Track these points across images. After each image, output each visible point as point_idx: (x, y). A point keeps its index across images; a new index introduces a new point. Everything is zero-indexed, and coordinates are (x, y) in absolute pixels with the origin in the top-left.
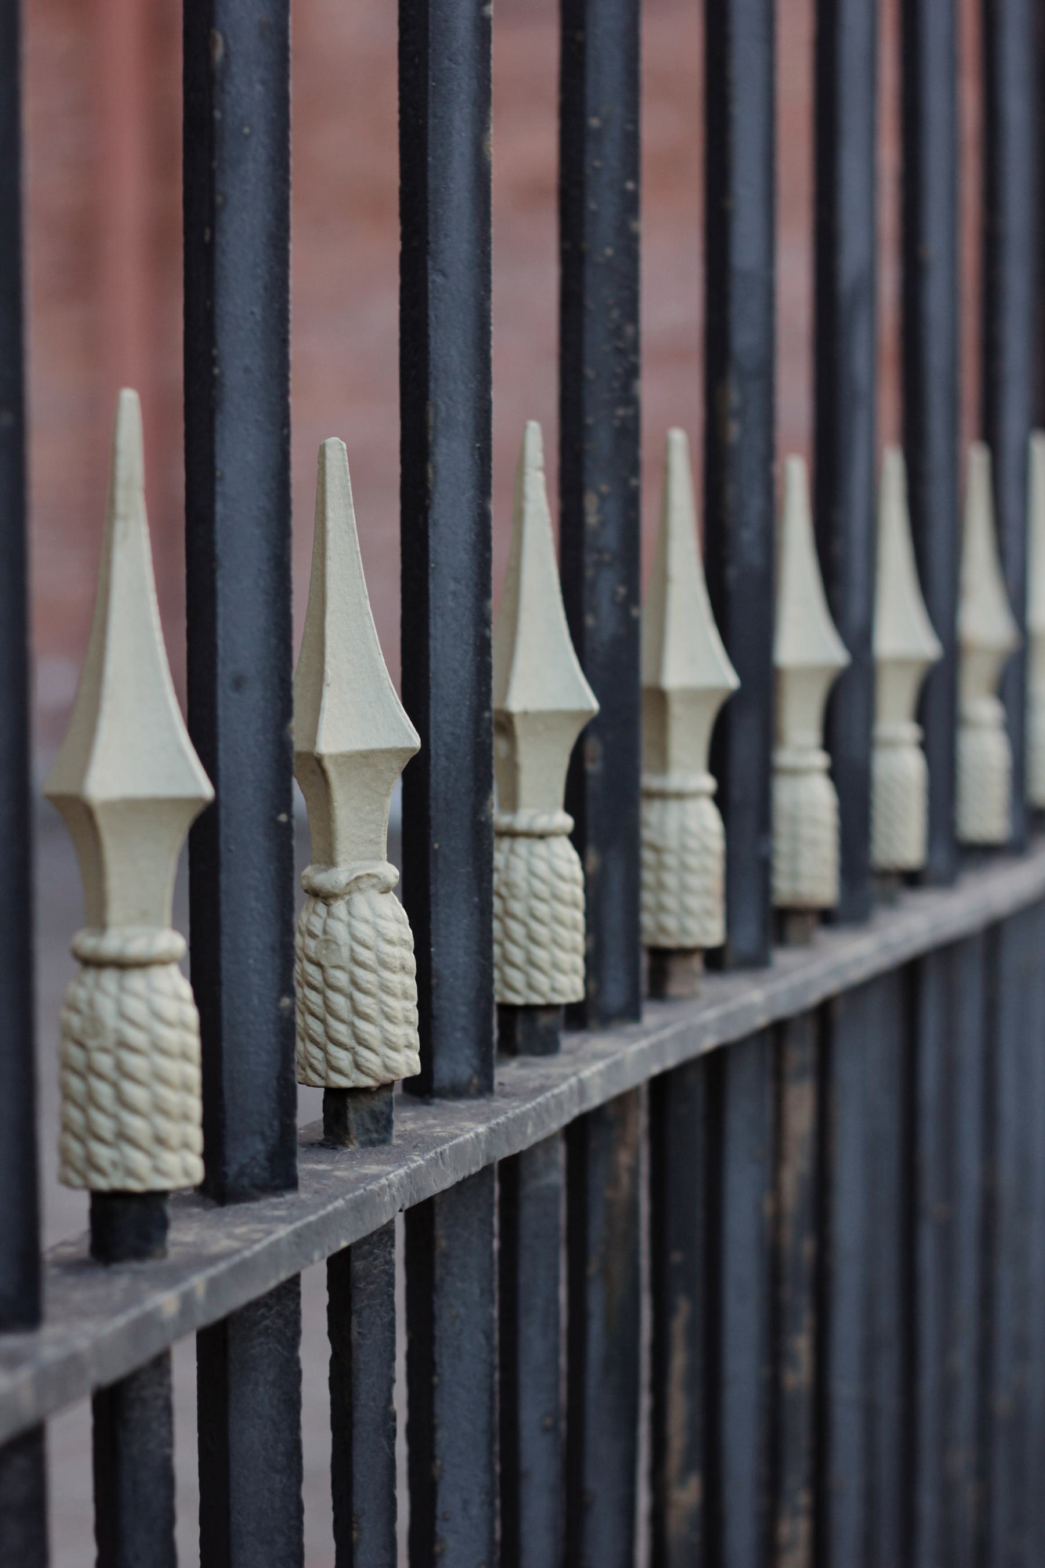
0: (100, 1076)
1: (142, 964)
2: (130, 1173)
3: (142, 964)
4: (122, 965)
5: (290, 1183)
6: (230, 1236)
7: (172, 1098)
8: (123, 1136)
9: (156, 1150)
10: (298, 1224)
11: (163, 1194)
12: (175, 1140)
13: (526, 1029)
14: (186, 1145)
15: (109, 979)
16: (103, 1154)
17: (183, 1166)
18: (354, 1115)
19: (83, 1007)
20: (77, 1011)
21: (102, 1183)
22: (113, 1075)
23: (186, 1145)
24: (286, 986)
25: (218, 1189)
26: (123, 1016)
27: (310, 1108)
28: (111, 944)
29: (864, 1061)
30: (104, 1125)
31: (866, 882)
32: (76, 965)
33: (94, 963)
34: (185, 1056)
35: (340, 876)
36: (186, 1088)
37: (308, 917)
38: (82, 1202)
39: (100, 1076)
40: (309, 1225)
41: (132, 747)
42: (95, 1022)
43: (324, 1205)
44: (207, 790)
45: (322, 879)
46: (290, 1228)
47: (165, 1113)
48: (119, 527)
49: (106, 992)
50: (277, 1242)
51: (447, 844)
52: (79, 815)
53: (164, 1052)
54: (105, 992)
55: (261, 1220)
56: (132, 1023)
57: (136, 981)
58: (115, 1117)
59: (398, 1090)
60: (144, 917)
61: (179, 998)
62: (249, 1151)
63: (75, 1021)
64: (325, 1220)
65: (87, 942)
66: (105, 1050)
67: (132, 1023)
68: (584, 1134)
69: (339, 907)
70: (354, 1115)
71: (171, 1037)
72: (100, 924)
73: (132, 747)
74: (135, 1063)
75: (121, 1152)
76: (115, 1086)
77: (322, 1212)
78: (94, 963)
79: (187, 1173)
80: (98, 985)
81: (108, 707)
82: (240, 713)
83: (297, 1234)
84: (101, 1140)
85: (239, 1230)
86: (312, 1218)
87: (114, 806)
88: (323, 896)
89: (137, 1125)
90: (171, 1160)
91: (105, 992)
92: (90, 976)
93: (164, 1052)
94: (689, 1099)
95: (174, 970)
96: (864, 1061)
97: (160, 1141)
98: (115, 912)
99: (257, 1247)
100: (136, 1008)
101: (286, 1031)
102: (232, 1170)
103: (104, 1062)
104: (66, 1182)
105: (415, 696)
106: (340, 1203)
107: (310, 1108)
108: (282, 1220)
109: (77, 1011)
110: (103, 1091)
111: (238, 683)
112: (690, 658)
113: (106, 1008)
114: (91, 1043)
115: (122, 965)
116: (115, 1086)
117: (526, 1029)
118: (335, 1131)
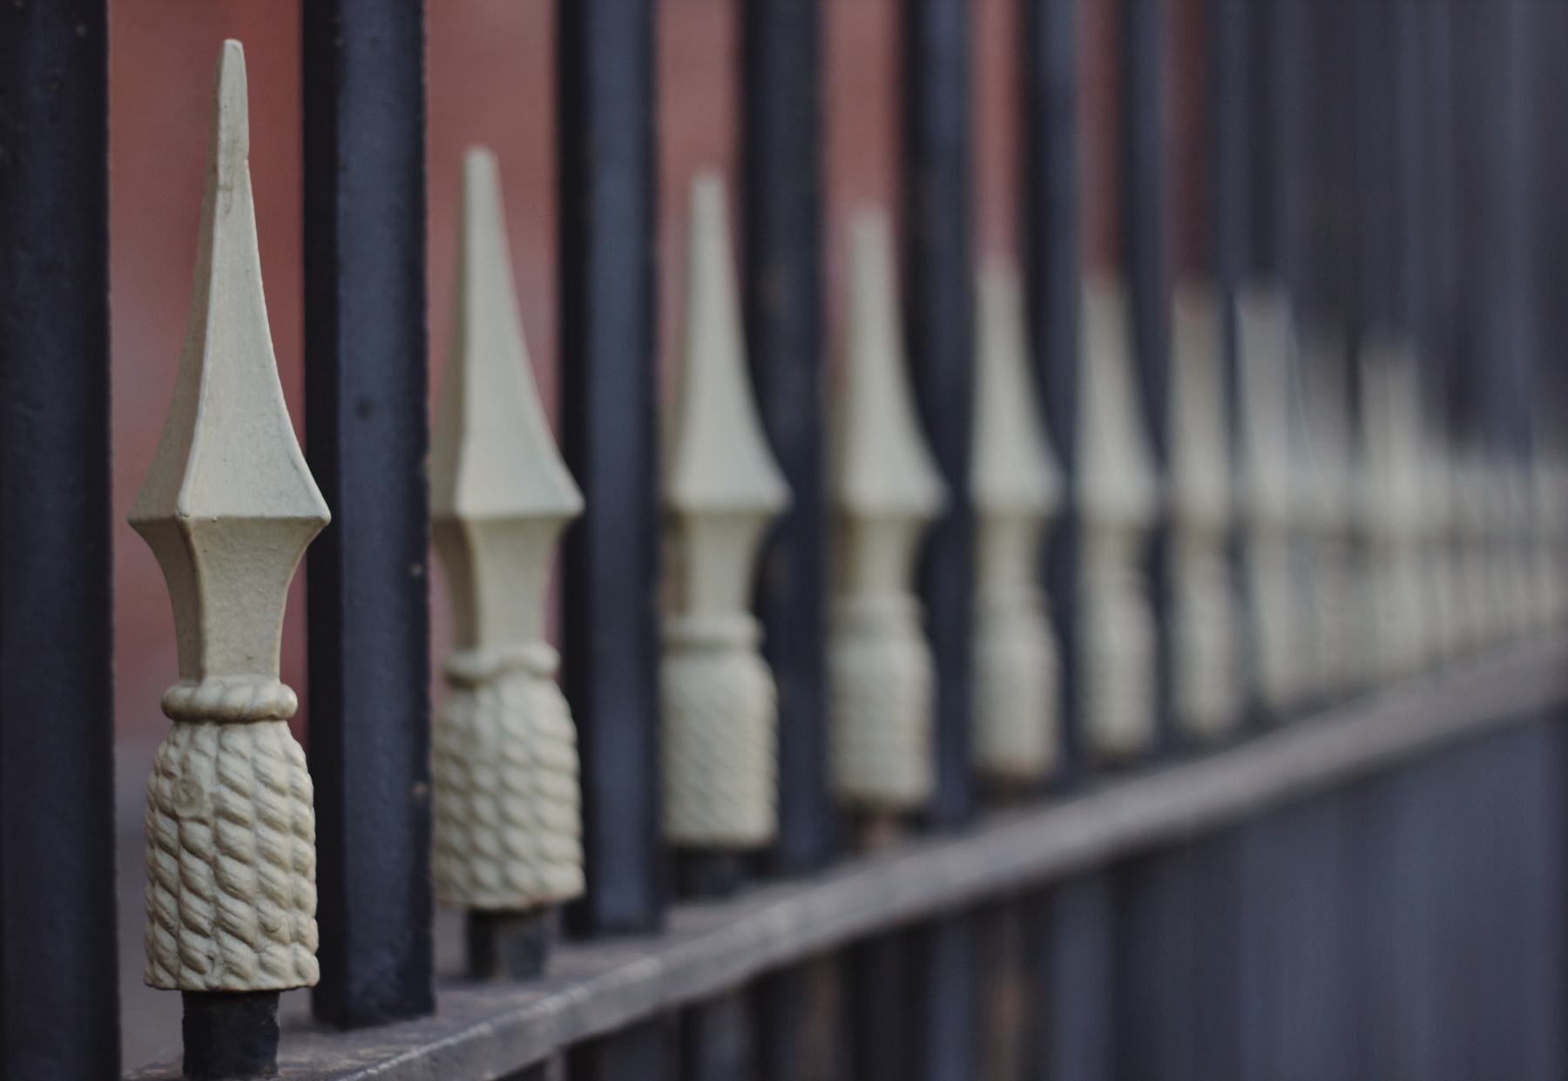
0: (195, 852)
1: (246, 719)
2: (231, 968)
3: (246, 719)
4: (224, 719)
5: (424, 1006)
6: (354, 1056)
7: (282, 879)
8: (223, 925)
9: (262, 940)
10: (434, 1046)
11: (273, 994)
12: (285, 931)
13: (701, 873)
14: (299, 938)
15: (206, 736)
16: (199, 946)
17: (293, 963)
18: (504, 941)
19: (176, 770)
20: (169, 775)
21: (197, 981)
22: (212, 851)
23: (299, 938)
24: (419, 769)
25: (337, 1005)
26: (222, 778)
27: (448, 946)
28: (209, 694)
29: (1081, 956)
30: (200, 911)
31: (1081, 764)
32: (171, 722)
33: (189, 717)
34: (298, 831)
35: (485, 659)
36: (300, 869)
37: (446, 709)
38: (175, 1007)
39: (195, 852)
40: (447, 1048)
41: (237, 455)
42: (189, 786)
43: (465, 1028)
44: (326, 514)
45: (466, 664)
46: (425, 1049)
47: (273, 897)
48: (221, 199)
49: (202, 754)
50: (409, 1063)
51: (612, 640)
52: (171, 538)
53: (272, 824)
54: (201, 752)
55: (390, 1042)
56: (234, 788)
57: (238, 738)
58: (214, 901)
59: (551, 923)
60: (249, 662)
61: (292, 760)
62: (376, 967)
63: (166, 786)
64: (468, 1046)
65: (181, 694)
66: (202, 822)
67: (234, 788)
68: (770, 992)
69: (485, 697)
70: (504, 941)
71: (282, 807)
72: (195, 672)
73: (237, 455)
74: (237, 836)
75: (219, 944)
76: (213, 864)
77: (463, 1036)
78: (189, 717)
79: (299, 972)
80: (192, 742)
81: (205, 410)
82: (367, 443)
83: (434, 1057)
84: (196, 930)
85: (363, 1052)
86: (451, 1041)
87: (209, 525)
88: (462, 684)
89: (240, 912)
90: (281, 955)
91: (201, 752)
92: (183, 736)
93: (272, 824)
94: (892, 965)
95: (284, 727)
96: (1081, 956)
97: (267, 930)
98: (214, 657)
99: (384, 1066)
100: (238, 770)
101: (421, 821)
102: (356, 987)
103: (200, 835)
104: (155, 984)
105: (574, 445)
106: (484, 1029)
107: (448, 946)
108: (417, 1042)
109: (169, 775)
110: (200, 871)
111: (364, 409)
112: (885, 471)
113: (203, 770)
114: (183, 813)
115: (224, 719)
116: (213, 864)
117: (701, 873)
118: (480, 966)
